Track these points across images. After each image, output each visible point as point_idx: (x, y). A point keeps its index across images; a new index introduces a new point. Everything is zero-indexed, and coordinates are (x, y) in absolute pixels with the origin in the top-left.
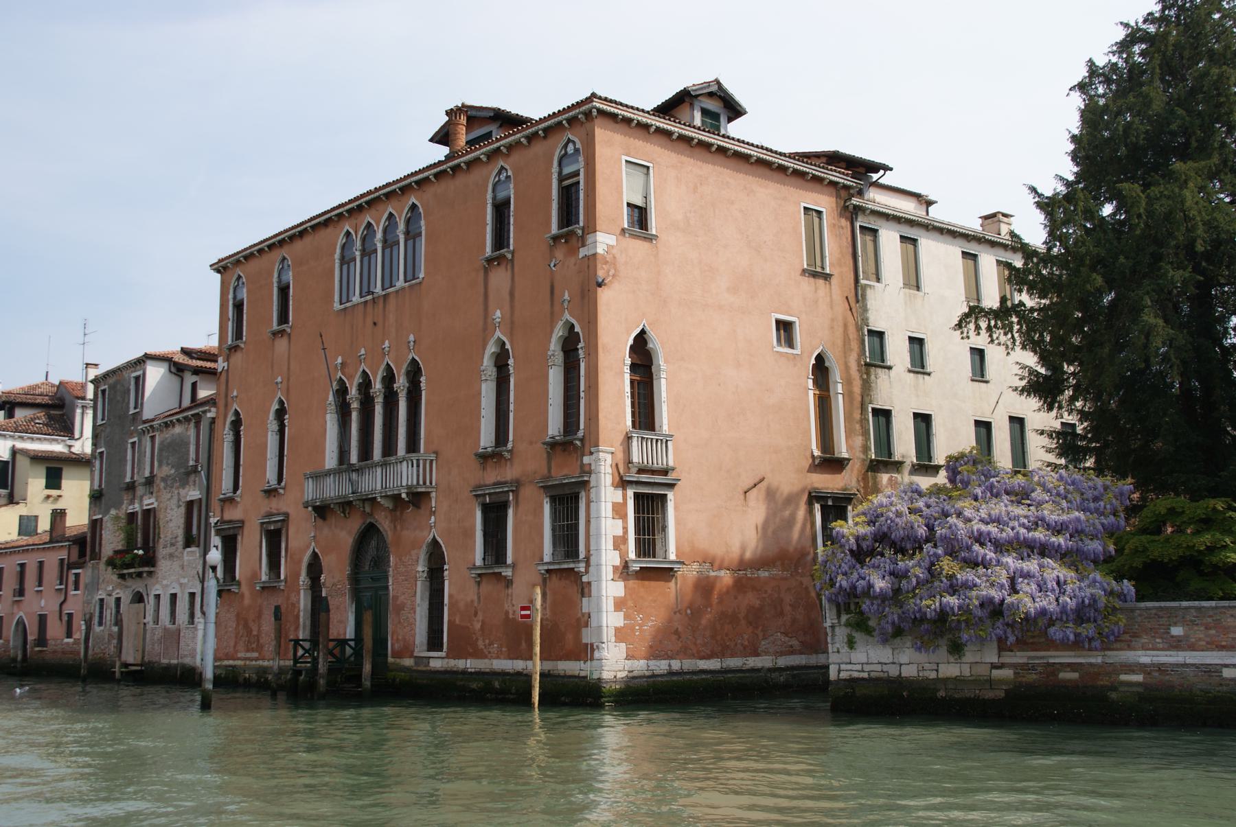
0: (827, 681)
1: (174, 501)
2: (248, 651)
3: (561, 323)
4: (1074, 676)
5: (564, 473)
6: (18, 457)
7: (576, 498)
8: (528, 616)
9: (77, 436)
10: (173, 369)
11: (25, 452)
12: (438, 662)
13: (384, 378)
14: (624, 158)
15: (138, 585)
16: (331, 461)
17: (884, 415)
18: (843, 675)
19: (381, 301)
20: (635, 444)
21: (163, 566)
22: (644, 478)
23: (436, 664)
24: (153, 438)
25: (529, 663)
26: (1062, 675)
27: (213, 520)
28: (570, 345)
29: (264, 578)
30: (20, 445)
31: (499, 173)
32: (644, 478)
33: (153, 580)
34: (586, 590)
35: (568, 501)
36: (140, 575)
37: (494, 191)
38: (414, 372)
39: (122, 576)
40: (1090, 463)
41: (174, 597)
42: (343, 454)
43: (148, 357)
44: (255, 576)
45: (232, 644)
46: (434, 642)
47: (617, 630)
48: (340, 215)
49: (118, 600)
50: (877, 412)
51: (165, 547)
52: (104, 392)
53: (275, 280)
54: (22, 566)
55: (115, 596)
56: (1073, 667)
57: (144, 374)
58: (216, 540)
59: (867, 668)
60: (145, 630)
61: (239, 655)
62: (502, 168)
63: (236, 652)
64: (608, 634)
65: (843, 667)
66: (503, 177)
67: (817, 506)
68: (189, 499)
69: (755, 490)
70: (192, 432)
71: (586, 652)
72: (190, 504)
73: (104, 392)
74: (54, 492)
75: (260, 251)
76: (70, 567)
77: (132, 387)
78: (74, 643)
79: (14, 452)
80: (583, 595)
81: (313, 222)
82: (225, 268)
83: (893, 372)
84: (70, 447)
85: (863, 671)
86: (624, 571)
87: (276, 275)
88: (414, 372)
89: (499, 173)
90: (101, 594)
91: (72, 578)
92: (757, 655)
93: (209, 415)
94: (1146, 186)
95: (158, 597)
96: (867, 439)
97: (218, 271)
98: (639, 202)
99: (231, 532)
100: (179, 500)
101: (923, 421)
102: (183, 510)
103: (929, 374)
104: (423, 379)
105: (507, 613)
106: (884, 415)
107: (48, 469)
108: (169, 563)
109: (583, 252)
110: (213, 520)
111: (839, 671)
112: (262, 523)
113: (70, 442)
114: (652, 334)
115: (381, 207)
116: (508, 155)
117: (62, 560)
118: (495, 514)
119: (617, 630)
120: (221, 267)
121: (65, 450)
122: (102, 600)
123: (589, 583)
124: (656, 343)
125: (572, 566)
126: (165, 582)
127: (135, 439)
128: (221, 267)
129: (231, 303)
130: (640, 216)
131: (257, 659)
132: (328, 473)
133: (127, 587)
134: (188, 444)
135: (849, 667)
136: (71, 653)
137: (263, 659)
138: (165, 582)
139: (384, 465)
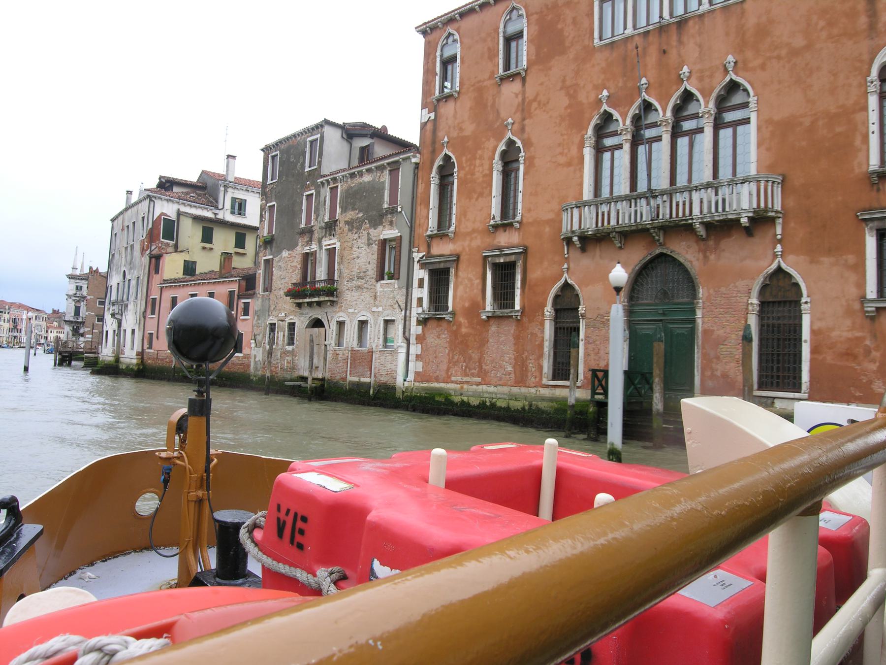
1: (364, 239)
2: (466, 375)
6: (181, 217)
9: (220, 207)
10: (345, 136)
11: (186, 214)
15: (318, 313)
16: (587, 194)
21: (349, 296)
24: (334, 190)
27: (417, 256)
29: (489, 308)
30: (184, 209)
31: (447, 38)
33: (334, 309)
36: (319, 304)
37: (441, 51)
39: (299, 305)
40: (371, 642)
41: (363, 324)
43: (327, 122)
44: (476, 307)
45: (444, 367)
49: (292, 326)
51: (351, 280)
52: (273, 157)
53: (438, 53)
54: (306, 256)
55: (288, 320)
57: (322, 137)
58: (420, 274)
60: (326, 351)
61: (453, 379)
63: (449, 377)
66: (450, 40)
68: (382, 237)
70: (386, 177)
72: (384, 242)
73: (273, 157)
74: (208, 245)
76: (239, 297)
77: (308, 150)
78: (244, 357)
79: (179, 214)
84: (216, 214)
86: (423, 322)
87: (502, 26)
89: (447, 38)
90: (272, 319)
91: (241, 306)
93: (414, 160)
95: (341, 324)
99: (442, 266)
100: (369, 239)
102: (375, 248)
107: (204, 227)
108: (356, 294)
110: (417, 256)
113: (217, 211)
117: (231, 293)
120: (428, 30)
121: (212, 216)
122: (273, 326)
126: (351, 310)
127: (313, 191)
128: (428, 30)
129: (438, 60)
131: (478, 384)
133: (301, 314)
134: (383, 189)
136: (242, 364)
137: (489, 384)
138: (351, 310)
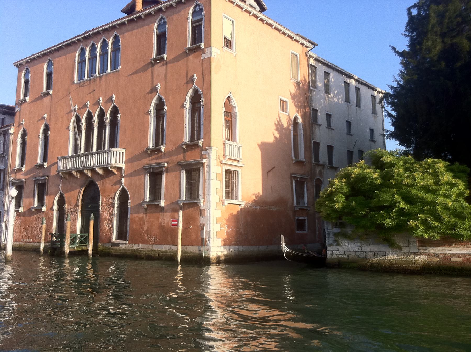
0: (325, 258)
3: (191, 90)
4: (460, 260)
5: (191, 157)
7: (198, 170)
8: (175, 225)
12: (125, 245)
13: (99, 115)
14: (224, 14)
17: (317, 145)
18: (335, 256)
19: (98, 79)
20: (227, 147)
22: (230, 162)
23: (122, 247)
25: (173, 248)
26: (453, 259)
28: (196, 98)
32: (230, 162)
34: (203, 213)
35: (194, 171)
38: (115, 112)
42: (76, 148)
46: (122, 235)
47: (218, 232)
48: (79, 40)
50: (315, 143)
56: (459, 255)
59: (347, 253)
62: (162, 18)
64: (213, 235)
65: (335, 252)
67: (294, 181)
69: (271, 172)
71: (201, 242)
75: (39, 57)
80: (201, 216)
81: (65, 44)
82: (21, 65)
83: (321, 127)
85: (345, 254)
88: (115, 112)
89: (160, 20)
92: (271, 244)
94: (424, 58)
96: (311, 154)
97: (17, 66)
98: (229, 37)
101: (330, 148)
103: (333, 130)
104: (119, 115)
105: (161, 223)
106: (317, 145)
109: (203, 57)
111: (332, 254)
112: (35, 181)
114: (232, 96)
115: (99, 37)
116: (165, 12)
118: (156, 176)
119: (218, 232)
120: (19, 66)
123: (204, 210)
124: (234, 102)
125: (196, 202)
128: (19, 66)
130: (228, 43)
132: (70, 157)
135: (338, 252)
139: (98, 153)
